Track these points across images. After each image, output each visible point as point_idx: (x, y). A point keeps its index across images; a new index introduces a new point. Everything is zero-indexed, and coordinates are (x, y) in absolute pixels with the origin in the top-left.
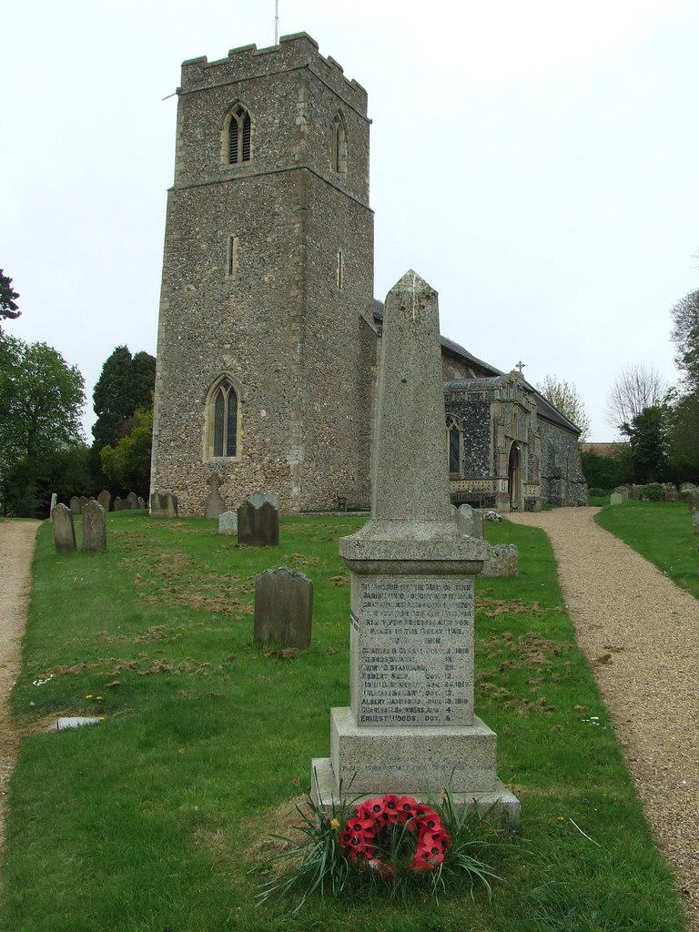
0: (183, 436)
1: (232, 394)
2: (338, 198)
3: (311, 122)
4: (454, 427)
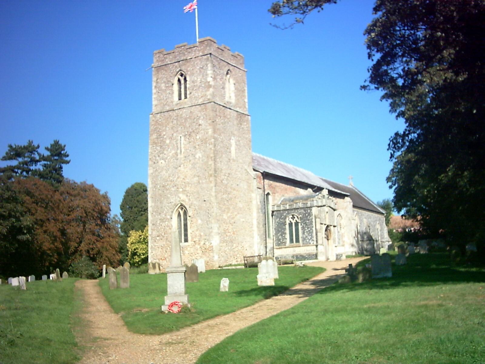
0: (163, 234)
1: (185, 213)
2: (230, 112)
3: (214, 79)
4: (296, 221)
